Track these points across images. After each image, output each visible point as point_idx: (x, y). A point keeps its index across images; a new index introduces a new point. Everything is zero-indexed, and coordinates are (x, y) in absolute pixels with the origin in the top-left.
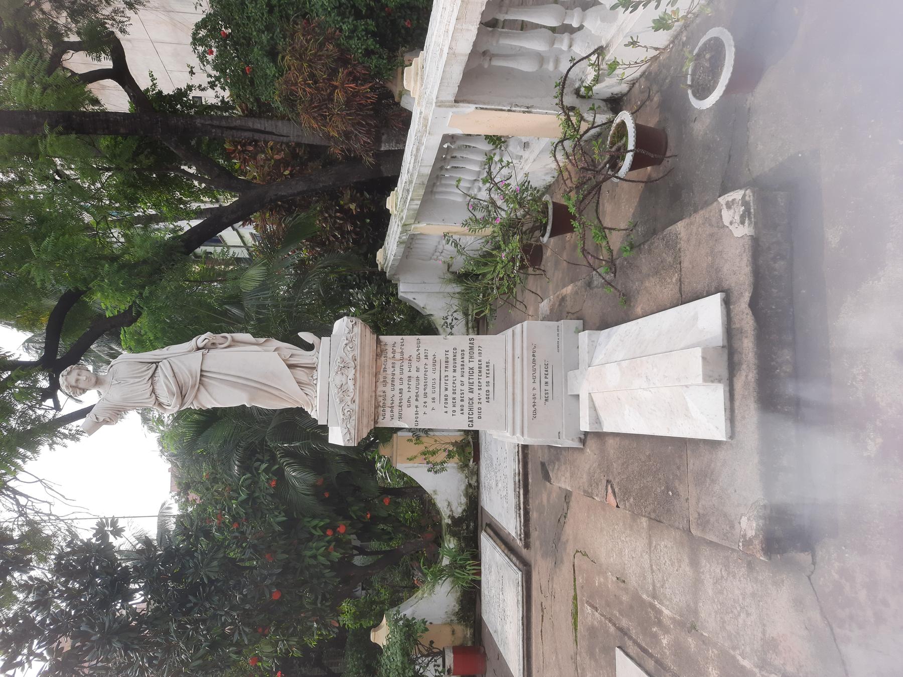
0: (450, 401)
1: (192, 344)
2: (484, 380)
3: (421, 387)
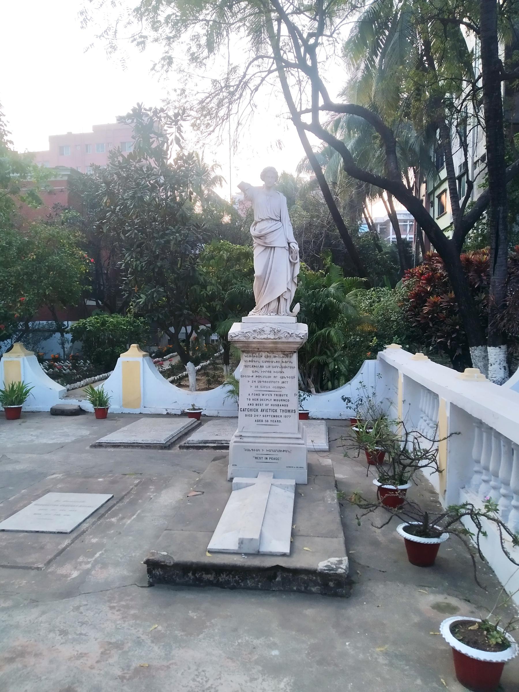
0: (256, 397)
1: (292, 239)
2: (269, 418)
3: (265, 379)
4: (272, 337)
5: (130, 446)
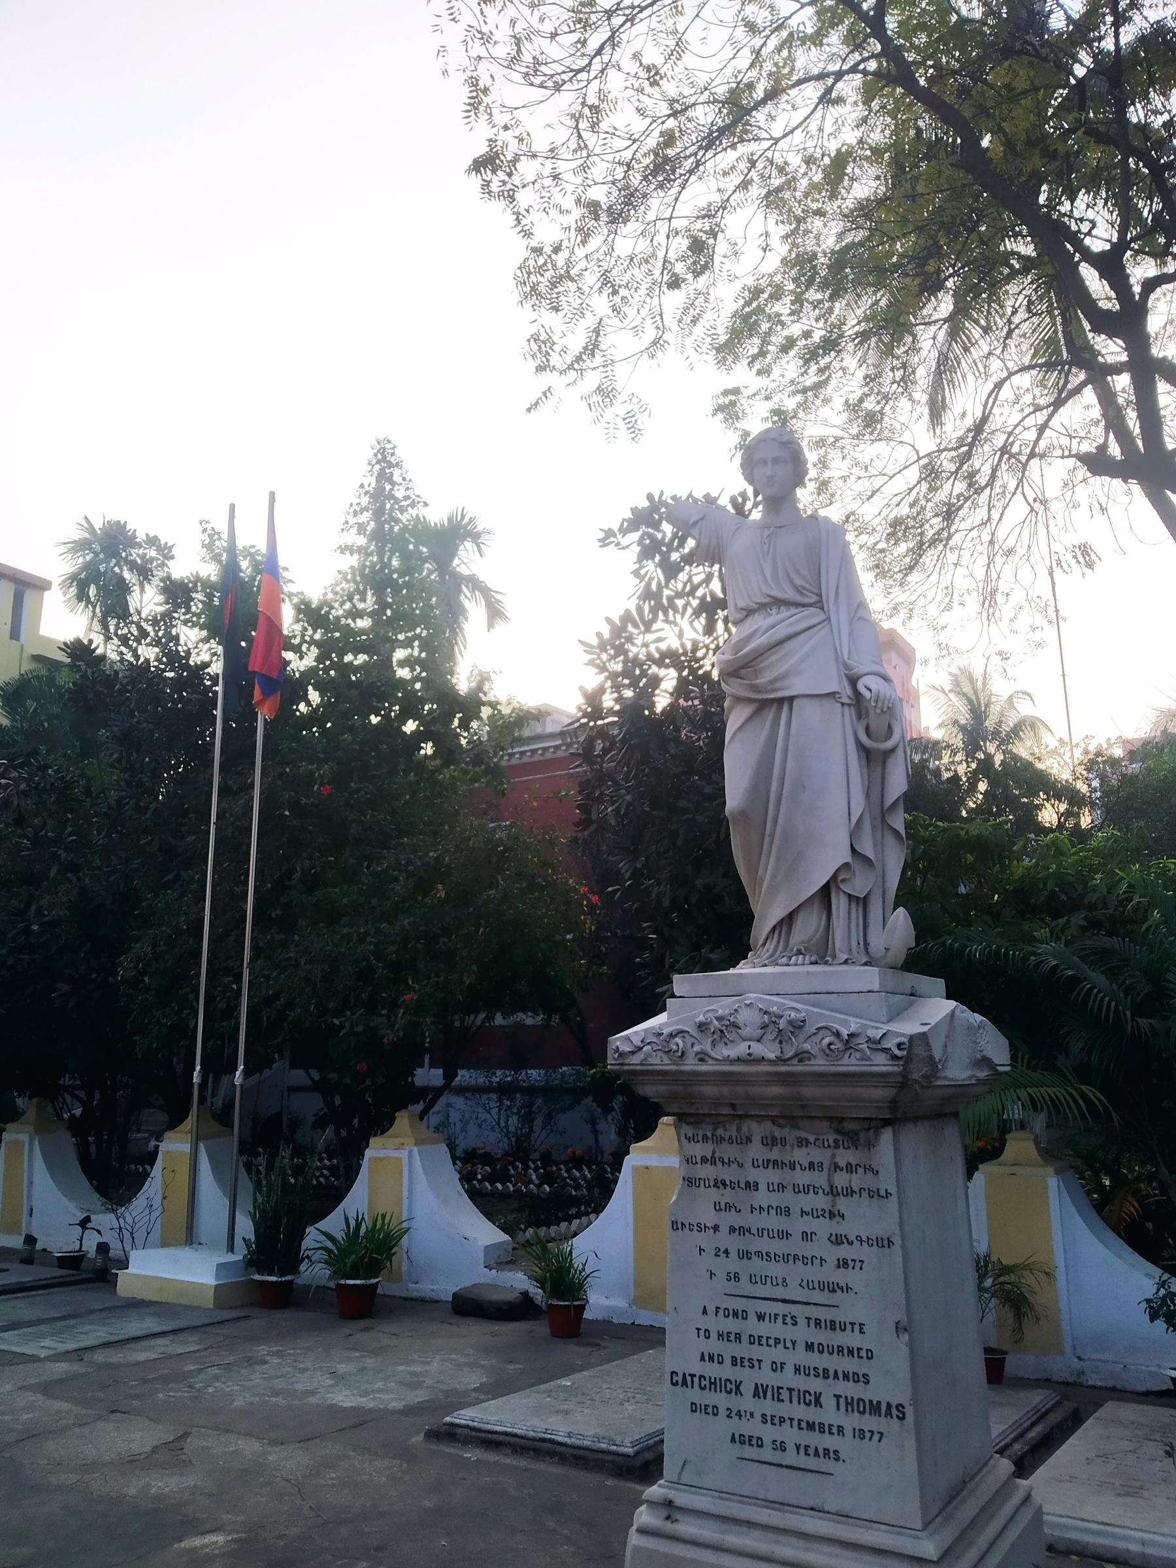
0: (732, 1325)
3: (764, 1244)
5: (529, 1449)
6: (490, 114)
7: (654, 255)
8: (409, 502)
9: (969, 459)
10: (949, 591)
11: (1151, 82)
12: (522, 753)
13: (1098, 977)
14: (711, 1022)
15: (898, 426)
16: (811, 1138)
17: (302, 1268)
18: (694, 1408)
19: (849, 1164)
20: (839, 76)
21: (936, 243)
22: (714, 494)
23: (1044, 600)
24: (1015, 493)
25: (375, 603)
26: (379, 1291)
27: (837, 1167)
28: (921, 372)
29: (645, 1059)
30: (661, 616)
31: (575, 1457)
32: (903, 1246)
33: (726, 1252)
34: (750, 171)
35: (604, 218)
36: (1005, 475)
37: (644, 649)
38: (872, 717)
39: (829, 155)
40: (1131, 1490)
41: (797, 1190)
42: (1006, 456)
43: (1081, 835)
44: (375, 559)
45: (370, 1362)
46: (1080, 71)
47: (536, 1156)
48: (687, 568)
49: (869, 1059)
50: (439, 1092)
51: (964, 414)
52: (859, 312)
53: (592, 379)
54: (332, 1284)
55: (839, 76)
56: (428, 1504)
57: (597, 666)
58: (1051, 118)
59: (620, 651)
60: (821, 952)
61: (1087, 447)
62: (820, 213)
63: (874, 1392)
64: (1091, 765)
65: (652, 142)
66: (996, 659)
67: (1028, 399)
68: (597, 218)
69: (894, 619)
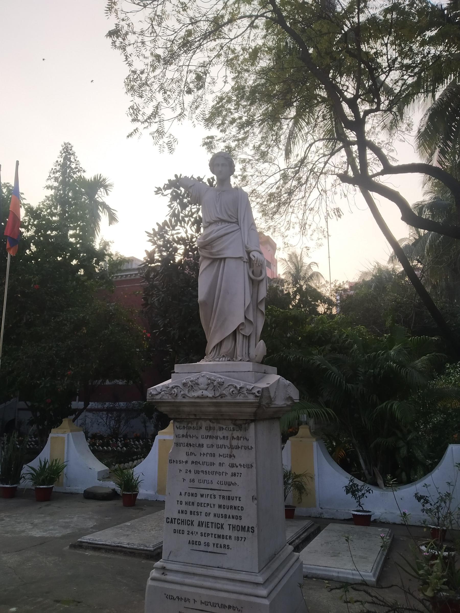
0: (191, 499)
3: (204, 468)
4: (209, 394)
6: (117, 13)
7: (181, 80)
8: (77, 170)
9: (299, 172)
10: (289, 222)
11: (370, 37)
12: (122, 276)
13: (334, 369)
14: (188, 383)
15: (273, 158)
16: (224, 427)
17: (21, 481)
18: (175, 531)
19: (238, 437)
20: (257, 17)
21: (290, 87)
22: (201, 177)
23: (323, 228)
24: (314, 187)
25: (61, 211)
26: (54, 490)
27: (233, 438)
28: (282, 137)
29: (162, 397)
30: (179, 224)
31: (131, 553)
32: (256, 468)
33: (190, 471)
34: (220, 50)
35: (162, 62)
36: (311, 180)
37: (172, 237)
38: (256, 266)
39: (252, 48)
40: (335, 554)
41: (218, 447)
42: (312, 173)
43: (332, 316)
44: (62, 192)
45: (48, 518)
46: (346, 29)
47: (121, 436)
48: (190, 206)
49: (247, 397)
50: (81, 411)
51: (297, 155)
52: (261, 112)
53: (154, 127)
54: (33, 488)
55: (257, 17)
56: (69, 573)
57: (152, 242)
58: (335, 45)
59: (162, 237)
60: (232, 356)
61: (341, 172)
62: (247, 71)
63: (245, 522)
64: (337, 291)
65: (182, 33)
66: (305, 250)
67: (321, 151)
68: (159, 62)
69: (268, 232)
